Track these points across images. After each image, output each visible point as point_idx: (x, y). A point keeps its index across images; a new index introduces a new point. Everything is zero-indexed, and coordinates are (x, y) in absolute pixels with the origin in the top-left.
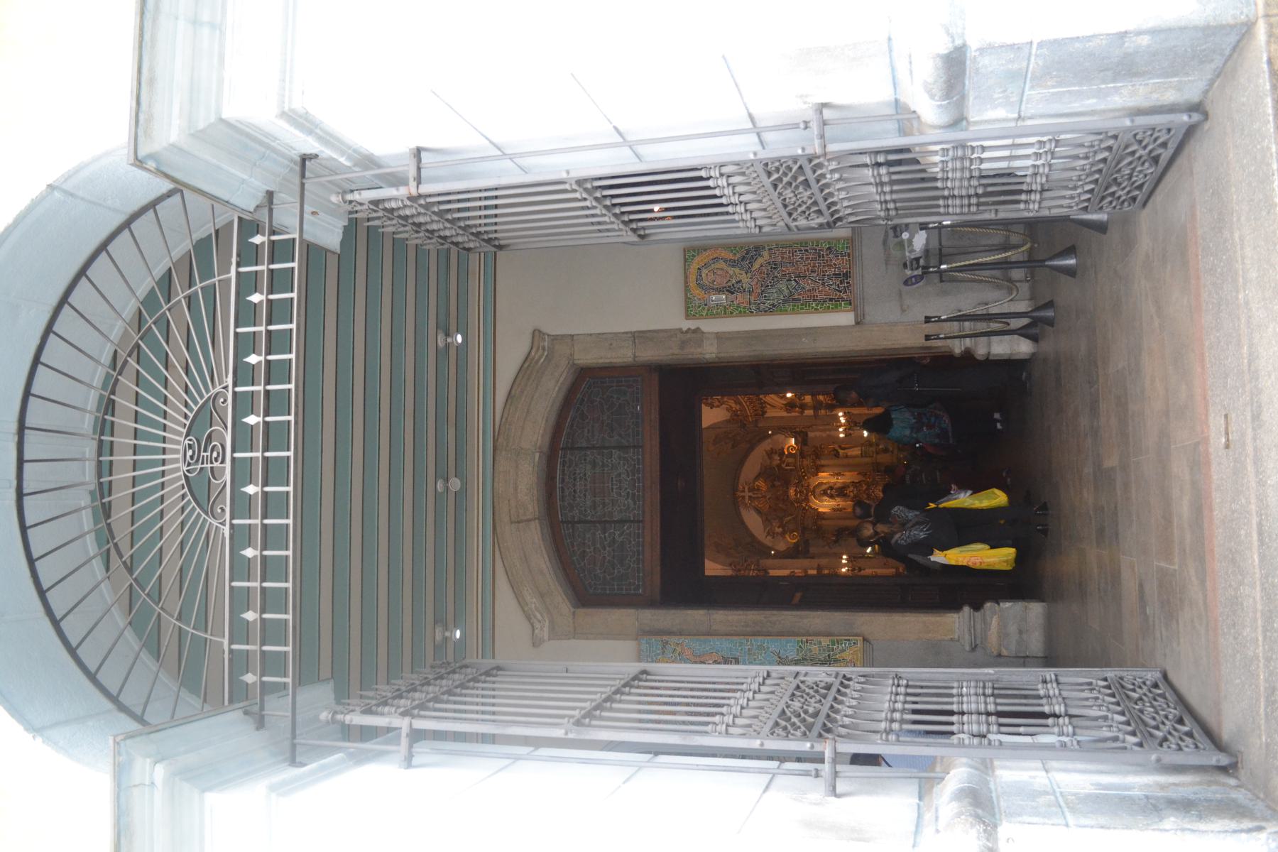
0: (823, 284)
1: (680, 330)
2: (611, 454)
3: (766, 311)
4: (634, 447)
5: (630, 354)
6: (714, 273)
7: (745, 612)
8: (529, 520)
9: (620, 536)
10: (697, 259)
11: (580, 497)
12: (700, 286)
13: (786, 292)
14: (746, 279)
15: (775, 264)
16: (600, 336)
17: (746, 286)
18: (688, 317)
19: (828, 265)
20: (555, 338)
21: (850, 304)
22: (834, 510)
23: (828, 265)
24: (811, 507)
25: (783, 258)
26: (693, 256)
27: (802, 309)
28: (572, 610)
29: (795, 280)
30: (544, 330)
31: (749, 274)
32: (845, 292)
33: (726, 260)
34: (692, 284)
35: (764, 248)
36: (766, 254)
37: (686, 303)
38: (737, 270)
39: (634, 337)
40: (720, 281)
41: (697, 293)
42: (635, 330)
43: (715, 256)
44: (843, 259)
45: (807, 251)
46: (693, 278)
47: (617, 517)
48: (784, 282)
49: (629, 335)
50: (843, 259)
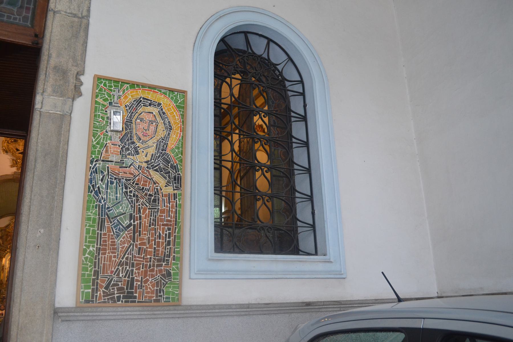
0: (120, 264)
3: (91, 182)
5: (59, 7)
6: (151, 122)
10: (173, 104)
12: (139, 102)
13: (115, 211)
14: (141, 159)
15: (154, 200)
17: (128, 161)
18: (98, 79)
19: (146, 272)
21: (87, 302)
22: (3, 266)
23: (146, 272)
24: (7, 254)
25: (163, 211)
26: (176, 101)
27: (88, 231)
29: (130, 225)
31: (145, 165)
32: (106, 294)
33: (166, 138)
34: (140, 93)
35: (177, 188)
36: (170, 190)
37: (117, 81)
38: (152, 151)
39: (83, 17)
40: (138, 128)
41: (131, 96)
42: (91, 20)
43: (174, 126)
44: (152, 292)
45: (169, 243)
46: (150, 95)
48: (129, 210)
49: (85, 13)
50: (152, 292)
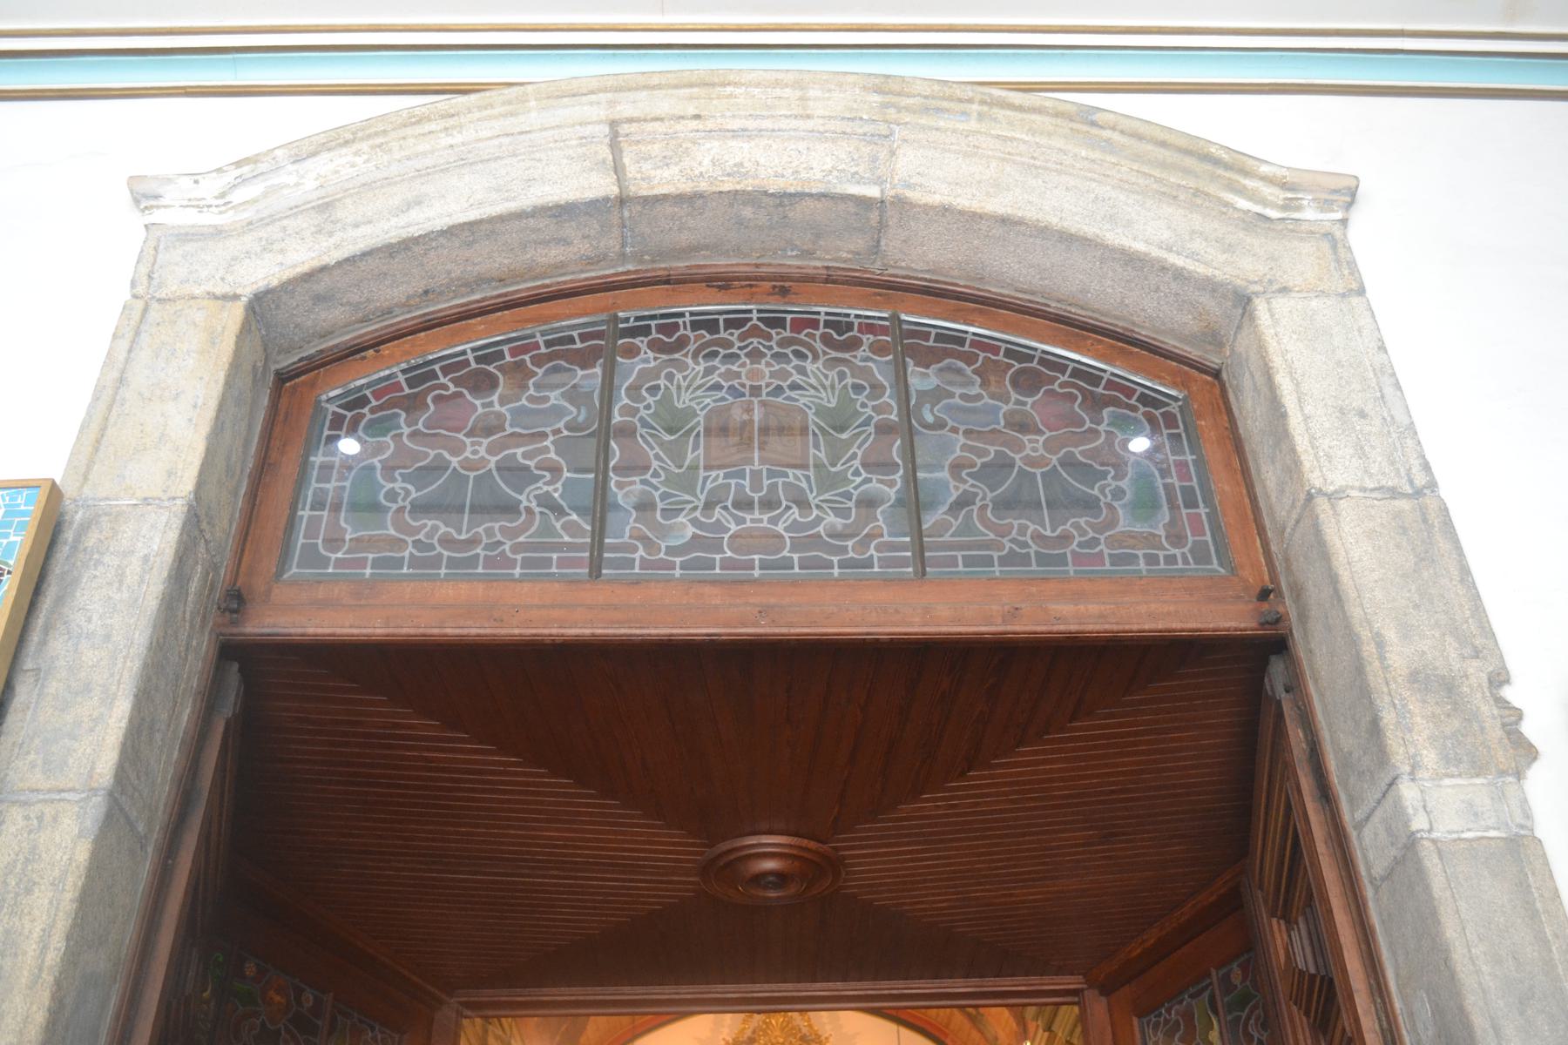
1: (1500, 678)
2: (887, 467)
4: (920, 548)
7: (48, 978)
8: (618, 169)
9: (546, 502)
11: (709, 371)
16: (1387, 381)
20: (1335, 243)
28: (247, 292)
30: (1358, 217)
47: (624, 492)
